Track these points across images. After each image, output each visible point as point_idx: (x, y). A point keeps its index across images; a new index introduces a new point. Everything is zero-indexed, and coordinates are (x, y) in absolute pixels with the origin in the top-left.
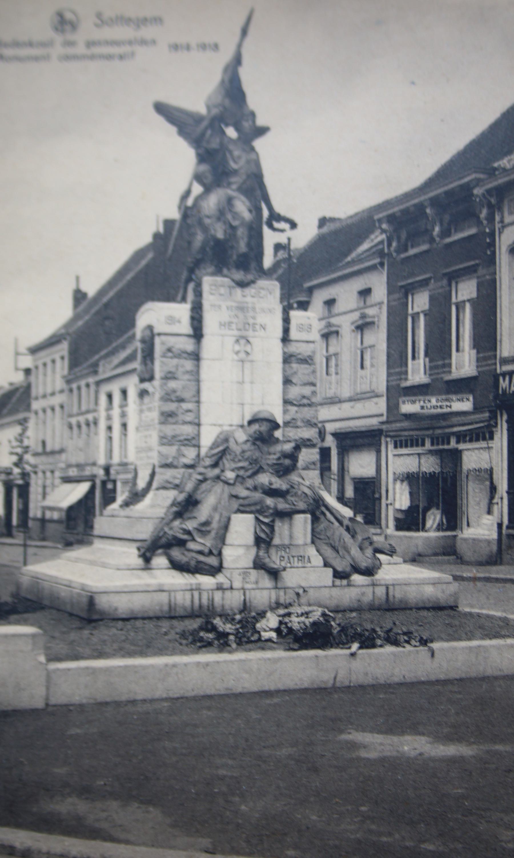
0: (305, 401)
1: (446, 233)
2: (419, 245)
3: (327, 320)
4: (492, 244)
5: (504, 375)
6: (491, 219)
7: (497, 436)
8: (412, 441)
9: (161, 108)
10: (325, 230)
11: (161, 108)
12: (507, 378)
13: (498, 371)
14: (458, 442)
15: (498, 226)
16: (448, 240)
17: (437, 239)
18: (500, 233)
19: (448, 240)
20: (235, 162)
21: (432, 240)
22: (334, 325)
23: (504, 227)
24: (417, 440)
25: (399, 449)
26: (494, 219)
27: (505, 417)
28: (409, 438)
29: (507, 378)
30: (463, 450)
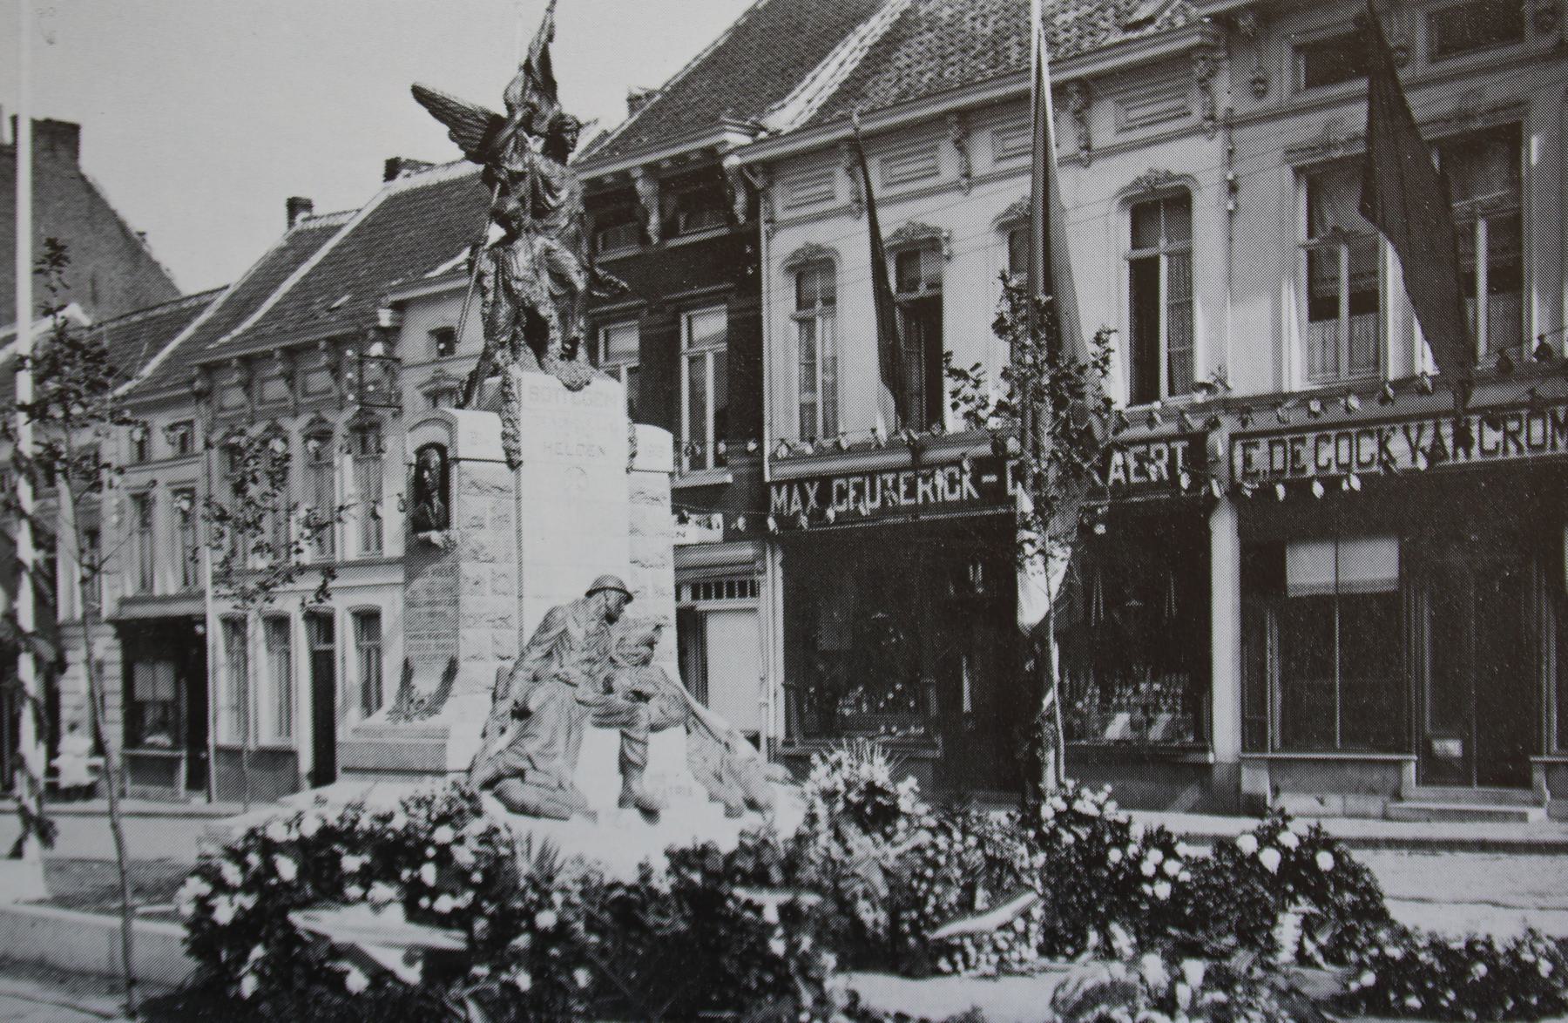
1: (668, 230)
2: (618, 245)
3: (437, 367)
4: (756, 259)
5: (779, 485)
6: (752, 211)
7: (765, 591)
8: (731, 585)
9: (421, 95)
10: (402, 184)
11: (421, 95)
12: (784, 489)
13: (767, 478)
14: (695, 596)
15: (764, 228)
16: (673, 243)
17: (655, 240)
18: (768, 238)
19: (673, 243)
20: (554, 197)
21: (644, 239)
22: (447, 378)
23: (774, 230)
24: (731, 585)
25: (725, 599)
26: (757, 215)
27: (779, 558)
28: (724, 580)
29: (784, 489)
30: (707, 612)
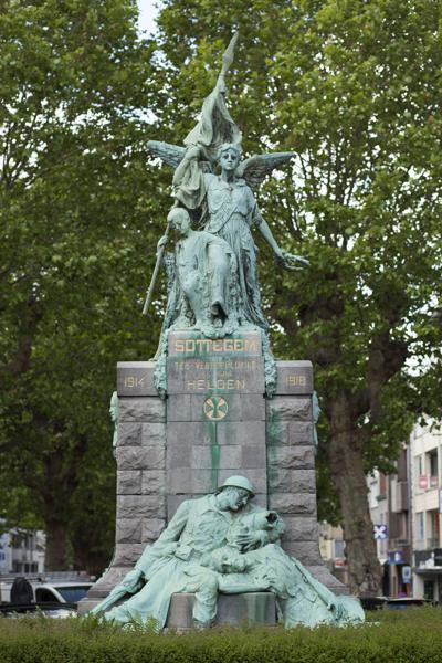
0: (297, 463)
